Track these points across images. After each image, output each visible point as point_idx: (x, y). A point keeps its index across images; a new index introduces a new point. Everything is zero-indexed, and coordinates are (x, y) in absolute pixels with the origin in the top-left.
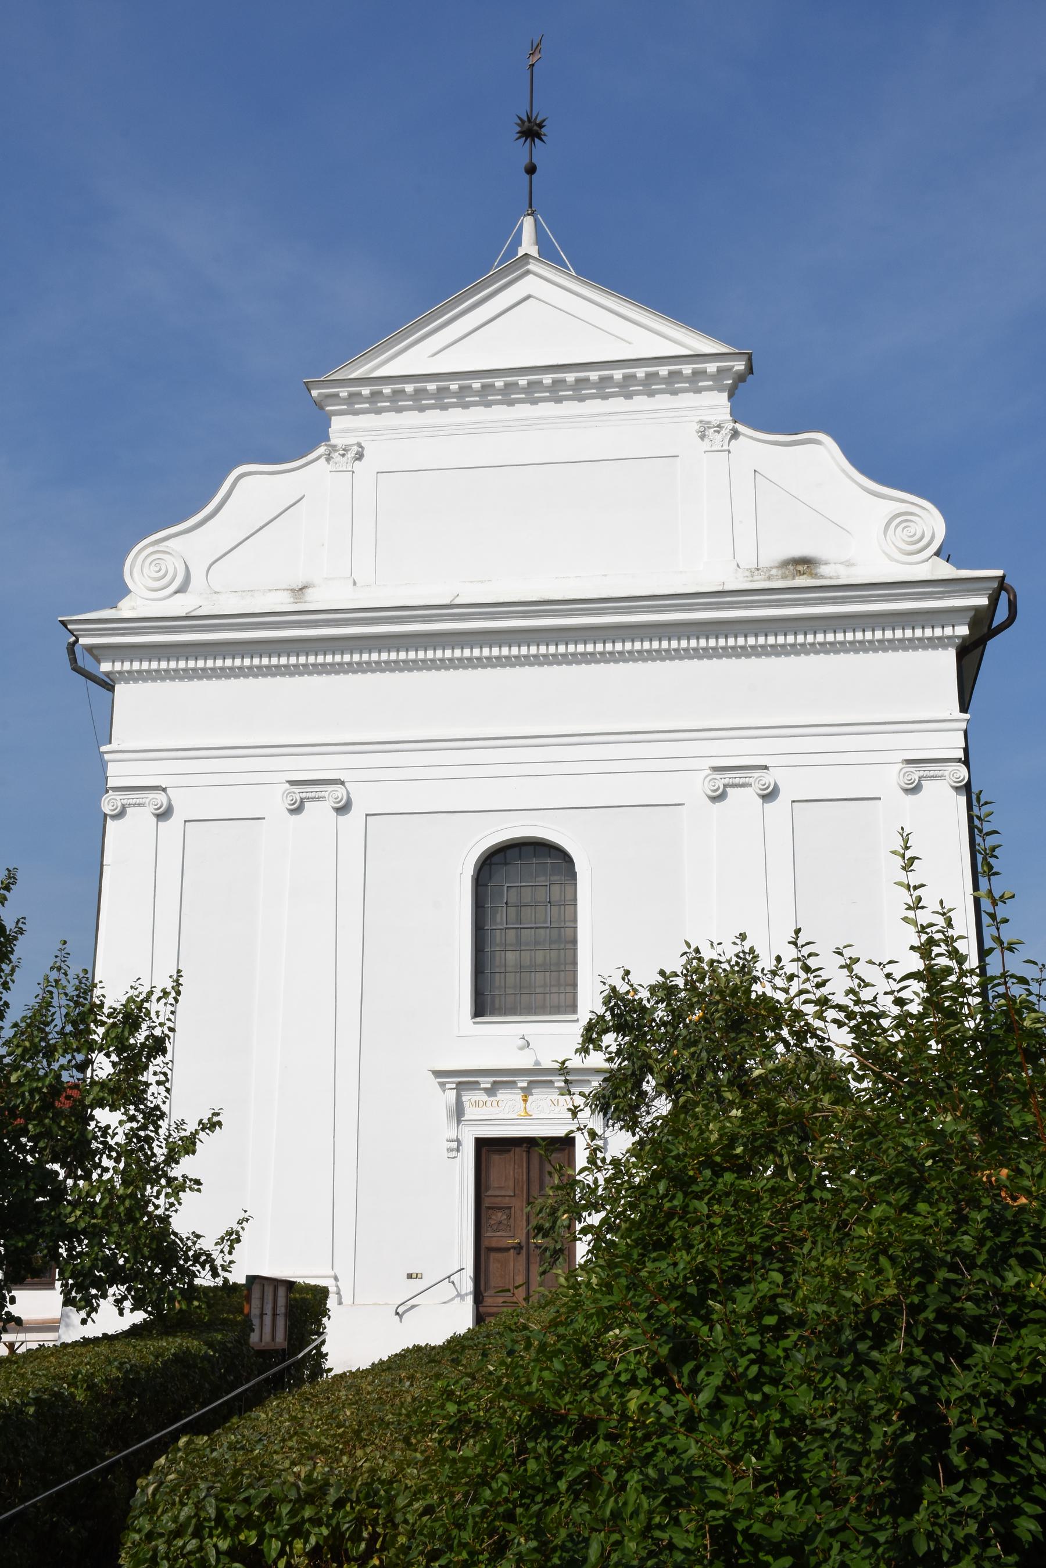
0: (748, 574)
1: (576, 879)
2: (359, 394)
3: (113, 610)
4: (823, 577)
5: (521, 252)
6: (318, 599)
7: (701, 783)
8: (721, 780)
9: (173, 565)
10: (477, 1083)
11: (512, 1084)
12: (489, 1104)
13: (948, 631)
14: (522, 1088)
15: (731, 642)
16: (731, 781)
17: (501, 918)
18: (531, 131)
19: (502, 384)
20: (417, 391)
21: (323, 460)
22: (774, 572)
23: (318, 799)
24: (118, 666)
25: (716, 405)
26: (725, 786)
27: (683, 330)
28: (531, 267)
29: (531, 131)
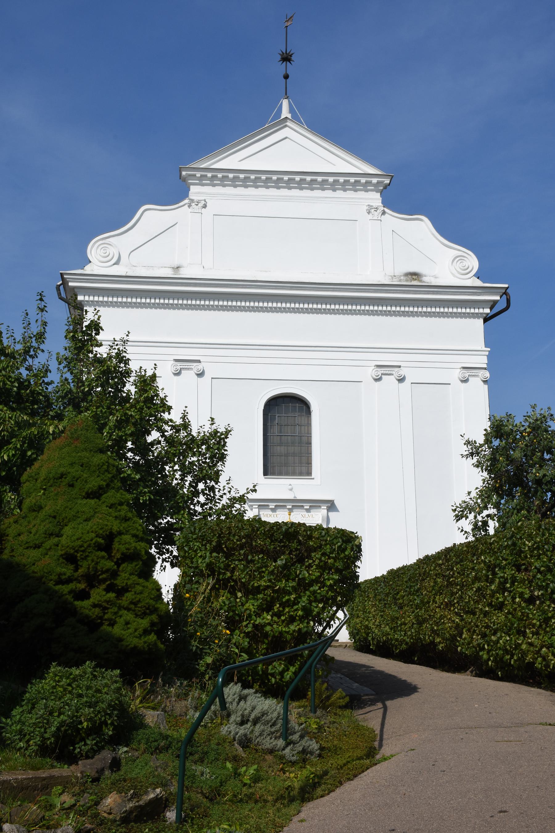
0: (390, 278)
1: (310, 414)
2: (206, 176)
3: (82, 270)
4: (424, 282)
5: (283, 117)
6: (185, 273)
7: (371, 372)
8: (381, 371)
9: (113, 251)
10: (268, 505)
11: (284, 507)
12: (272, 516)
13: (481, 311)
14: (289, 509)
15: (248, 304)
16: (384, 372)
17: (275, 430)
18: (286, 58)
19: (265, 178)
20: (234, 177)
21: (187, 206)
22: (402, 278)
23: (188, 369)
24: (87, 298)
25: (375, 198)
26: (382, 374)
27: (360, 162)
28: (288, 124)
29: (286, 58)
